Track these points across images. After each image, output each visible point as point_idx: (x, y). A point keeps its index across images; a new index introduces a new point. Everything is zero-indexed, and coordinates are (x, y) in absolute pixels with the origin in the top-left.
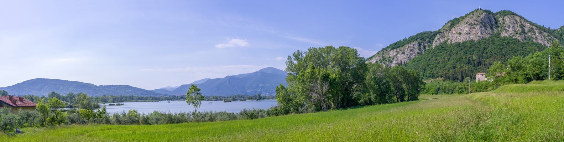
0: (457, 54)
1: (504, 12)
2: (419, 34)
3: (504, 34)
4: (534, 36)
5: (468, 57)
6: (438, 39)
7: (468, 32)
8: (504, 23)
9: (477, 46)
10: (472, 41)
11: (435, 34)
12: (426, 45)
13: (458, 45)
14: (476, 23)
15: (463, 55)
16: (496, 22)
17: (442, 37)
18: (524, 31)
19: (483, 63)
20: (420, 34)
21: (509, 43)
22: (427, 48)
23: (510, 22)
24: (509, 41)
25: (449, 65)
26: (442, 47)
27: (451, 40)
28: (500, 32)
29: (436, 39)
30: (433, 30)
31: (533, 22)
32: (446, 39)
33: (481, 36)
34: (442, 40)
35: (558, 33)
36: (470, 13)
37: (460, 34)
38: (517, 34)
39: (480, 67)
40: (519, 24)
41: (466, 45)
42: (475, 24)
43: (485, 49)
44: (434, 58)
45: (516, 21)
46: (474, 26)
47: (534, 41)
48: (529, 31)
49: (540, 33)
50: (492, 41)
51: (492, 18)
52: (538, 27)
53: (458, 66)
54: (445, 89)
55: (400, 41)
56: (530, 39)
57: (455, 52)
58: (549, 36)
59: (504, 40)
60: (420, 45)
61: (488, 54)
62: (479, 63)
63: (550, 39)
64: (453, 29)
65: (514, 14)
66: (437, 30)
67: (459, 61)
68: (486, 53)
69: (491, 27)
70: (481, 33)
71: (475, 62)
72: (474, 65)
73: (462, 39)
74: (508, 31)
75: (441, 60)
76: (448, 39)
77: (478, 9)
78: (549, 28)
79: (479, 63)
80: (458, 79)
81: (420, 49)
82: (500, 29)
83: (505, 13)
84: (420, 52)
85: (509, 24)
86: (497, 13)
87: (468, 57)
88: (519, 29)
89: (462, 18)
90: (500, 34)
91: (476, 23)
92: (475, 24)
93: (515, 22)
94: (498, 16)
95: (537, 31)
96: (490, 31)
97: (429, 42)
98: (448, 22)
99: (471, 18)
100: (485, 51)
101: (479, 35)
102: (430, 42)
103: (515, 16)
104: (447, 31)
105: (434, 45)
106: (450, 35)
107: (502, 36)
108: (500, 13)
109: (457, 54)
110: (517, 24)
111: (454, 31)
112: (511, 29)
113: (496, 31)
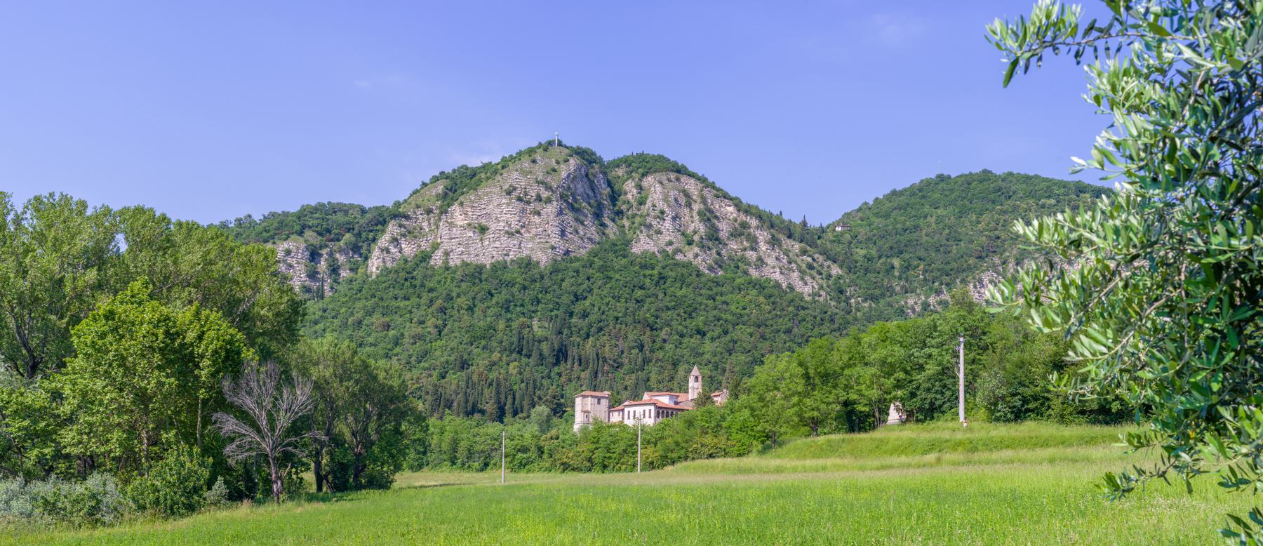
0: (471, 309)
1: (642, 158)
2: (318, 208)
3: (643, 245)
4: (751, 255)
5: (515, 325)
6: (395, 240)
7: (515, 226)
8: (642, 202)
9: (547, 282)
10: (527, 264)
11: (380, 219)
12: (341, 258)
13: (475, 274)
14: (545, 194)
15: (498, 316)
16: (614, 198)
17: (409, 233)
18: (714, 236)
19: (572, 352)
20: (316, 209)
21: (662, 278)
22: (345, 274)
23: (666, 199)
24: (663, 273)
25: (441, 353)
26: (411, 277)
27: (447, 254)
28: (629, 235)
29: (384, 241)
30: (371, 199)
31: (746, 200)
32: (425, 246)
33: (561, 246)
34: (408, 249)
35: (838, 239)
36: (520, 154)
37: (483, 230)
38: (690, 243)
39: (562, 368)
40: (696, 207)
41: (507, 277)
42: (539, 198)
43: (577, 298)
44: (377, 319)
45: (687, 195)
46: (538, 206)
47: (754, 273)
48: (734, 234)
49: (774, 242)
50: (603, 269)
51: (600, 181)
52: (769, 221)
53: (480, 362)
54: (455, 444)
55: (224, 225)
56: (738, 264)
57: (463, 301)
58: (804, 252)
59: (644, 267)
60: (314, 255)
61: (592, 318)
62: (561, 354)
63: (810, 267)
64: (455, 208)
65: (680, 170)
66: (389, 204)
67: (483, 337)
68: (585, 315)
69: (598, 216)
70: (563, 233)
71: (545, 347)
72: (541, 357)
73: (488, 252)
74: (659, 232)
75: (411, 330)
76: (436, 247)
77: (550, 143)
78: (804, 224)
79: (561, 354)
80: (482, 412)
81: (313, 275)
82: (626, 223)
83: (645, 165)
84: (314, 286)
85: (661, 205)
86: (617, 164)
87: (515, 325)
88: (697, 226)
89: (491, 171)
90: (628, 243)
91: (545, 194)
92: (539, 198)
93: (683, 200)
94: (620, 172)
95: (763, 236)
96: (592, 231)
97: (356, 248)
98: (435, 179)
99: (524, 173)
100: (579, 308)
101: (555, 240)
102: (359, 250)
103: (684, 178)
104: (429, 212)
105: (374, 265)
106: (443, 230)
107: (637, 249)
108: (626, 161)
109: (471, 309)
110: (689, 205)
111: (458, 215)
112: (668, 224)
113: (612, 230)
